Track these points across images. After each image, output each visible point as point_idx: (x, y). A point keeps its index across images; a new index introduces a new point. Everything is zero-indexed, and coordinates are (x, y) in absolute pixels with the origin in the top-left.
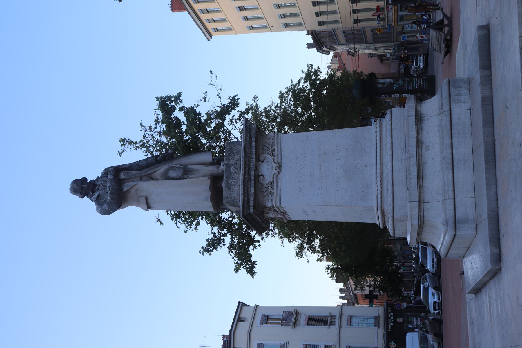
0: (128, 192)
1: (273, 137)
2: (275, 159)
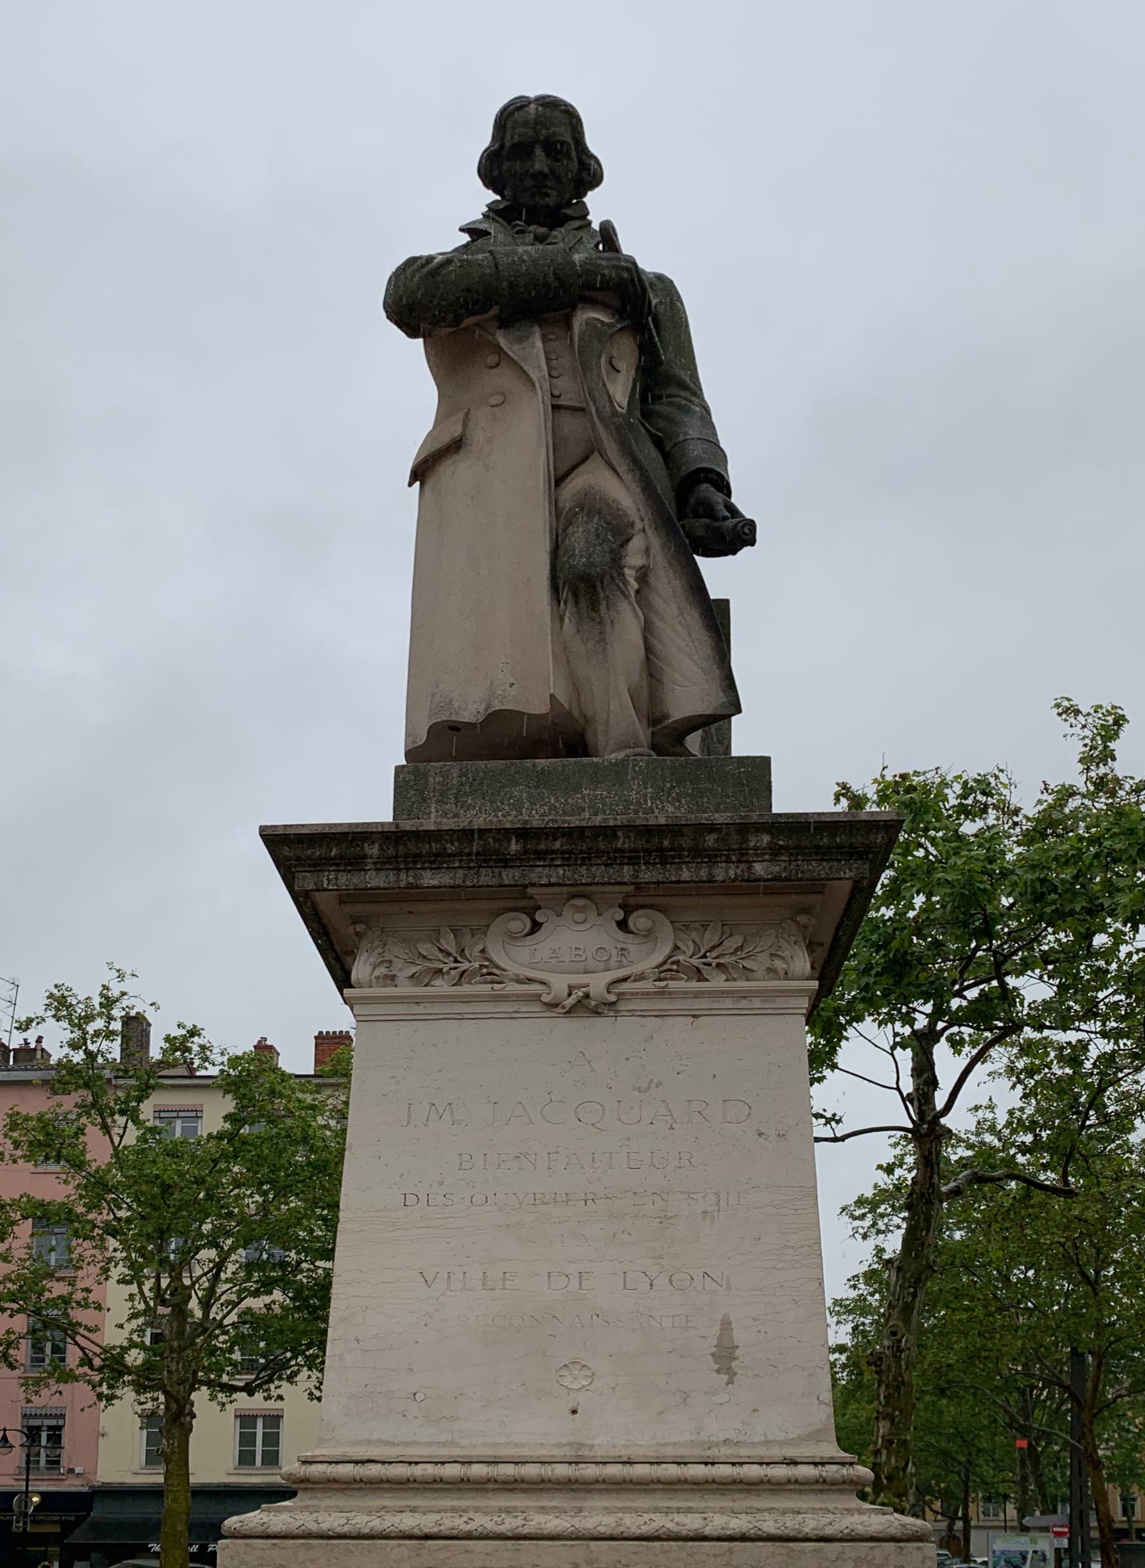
1: (782, 973)
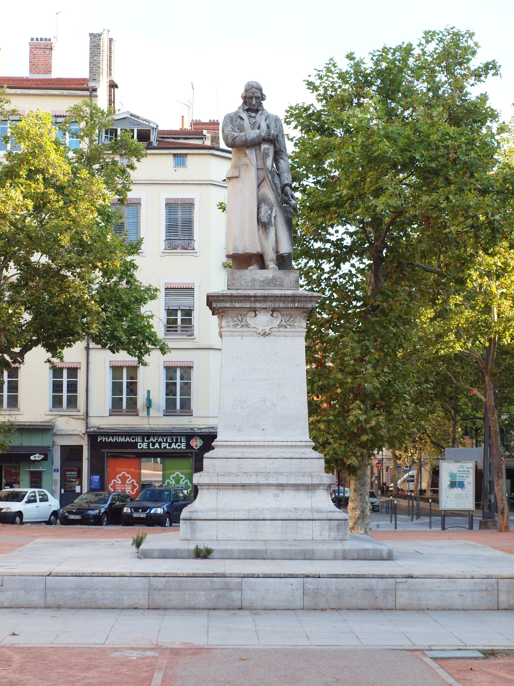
0: (245, 155)
2: (275, 329)
